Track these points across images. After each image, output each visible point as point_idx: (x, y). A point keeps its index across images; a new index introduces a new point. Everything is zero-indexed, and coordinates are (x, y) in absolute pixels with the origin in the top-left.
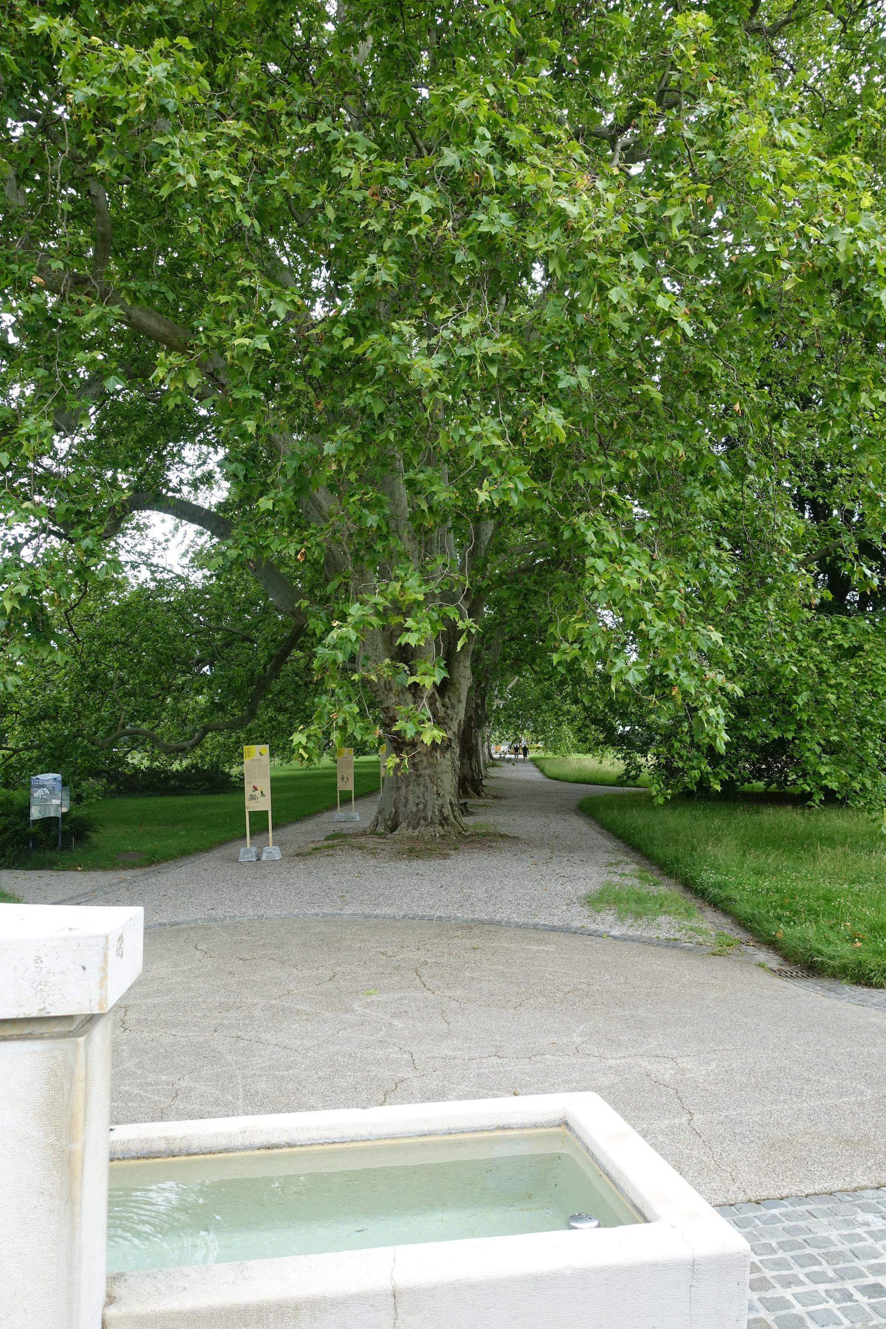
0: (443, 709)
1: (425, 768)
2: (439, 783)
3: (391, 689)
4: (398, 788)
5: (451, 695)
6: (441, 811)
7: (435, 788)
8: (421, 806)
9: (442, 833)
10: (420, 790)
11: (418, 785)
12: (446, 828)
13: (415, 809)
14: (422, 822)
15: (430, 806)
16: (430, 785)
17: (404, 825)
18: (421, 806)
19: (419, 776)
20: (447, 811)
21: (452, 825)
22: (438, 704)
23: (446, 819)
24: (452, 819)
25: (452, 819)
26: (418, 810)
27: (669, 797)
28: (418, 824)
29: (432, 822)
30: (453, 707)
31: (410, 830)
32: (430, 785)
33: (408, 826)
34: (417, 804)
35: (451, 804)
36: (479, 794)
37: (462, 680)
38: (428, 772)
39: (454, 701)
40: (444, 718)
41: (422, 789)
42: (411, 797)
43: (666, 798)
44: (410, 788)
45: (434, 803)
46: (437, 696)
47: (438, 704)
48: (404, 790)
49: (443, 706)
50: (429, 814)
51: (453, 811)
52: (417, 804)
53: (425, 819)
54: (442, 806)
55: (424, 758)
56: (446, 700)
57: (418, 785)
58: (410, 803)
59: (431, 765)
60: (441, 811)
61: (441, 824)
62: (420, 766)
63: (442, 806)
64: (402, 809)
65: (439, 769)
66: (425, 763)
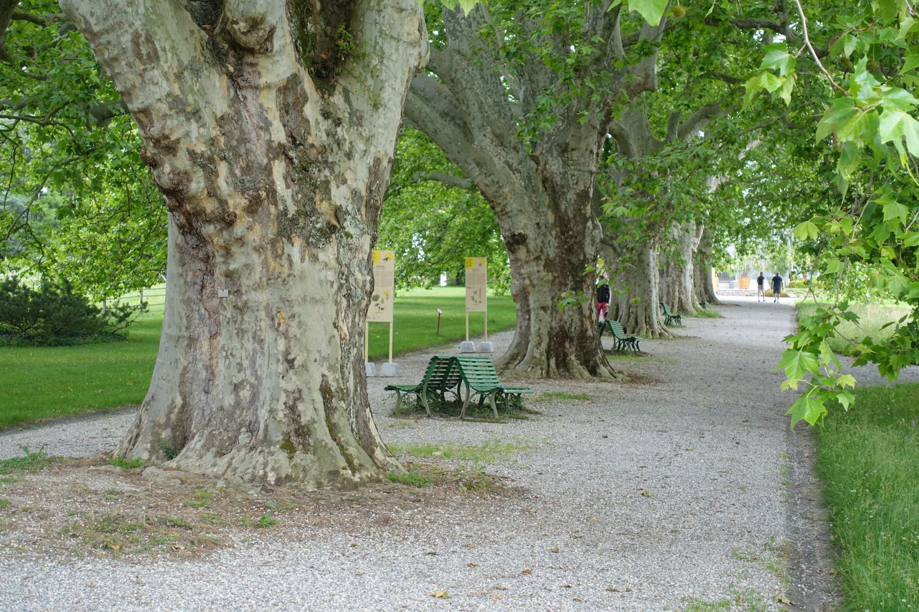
0: (325, 125)
1: (258, 287)
2: (294, 330)
3: (154, 57)
4: (192, 341)
5: (355, 87)
6: (292, 409)
7: (282, 345)
8: (245, 393)
9: (287, 470)
10: (243, 349)
11: (241, 333)
12: (299, 456)
13: (229, 400)
14: (243, 438)
15: (265, 395)
16: (269, 336)
17: (196, 443)
18: (245, 393)
19: (241, 309)
20: (311, 410)
21: (318, 449)
22: (311, 111)
23: (303, 432)
24: (322, 432)
25: (322, 432)
26: (238, 404)
27: (845, 401)
28: (234, 441)
29: (267, 440)
30: (357, 120)
31: (209, 457)
32: (269, 336)
33: (206, 447)
34: (237, 387)
35: (325, 391)
36: (593, 371)
37: (389, 47)
38: (261, 297)
39: (361, 103)
40: (324, 150)
41: (250, 345)
42: (221, 367)
43: (834, 407)
44: (221, 340)
45: (275, 387)
46: (308, 85)
47: (311, 111)
48: (205, 344)
49: (326, 115)
50: (263, 414)
51: (329, 410)
52: (237, 387)
53: (252, 430)
54: (298, 395)
55: (256, 259)
56: (337, 99)
57: (241, 333)
58: (219, 381)
59: (271, 278)
60: (292, 409)
61: (288, 447)
62: (245, 282)
63: (298, 395)
64: (198, 398)
65: (295, 292)
66: (258, 273)
